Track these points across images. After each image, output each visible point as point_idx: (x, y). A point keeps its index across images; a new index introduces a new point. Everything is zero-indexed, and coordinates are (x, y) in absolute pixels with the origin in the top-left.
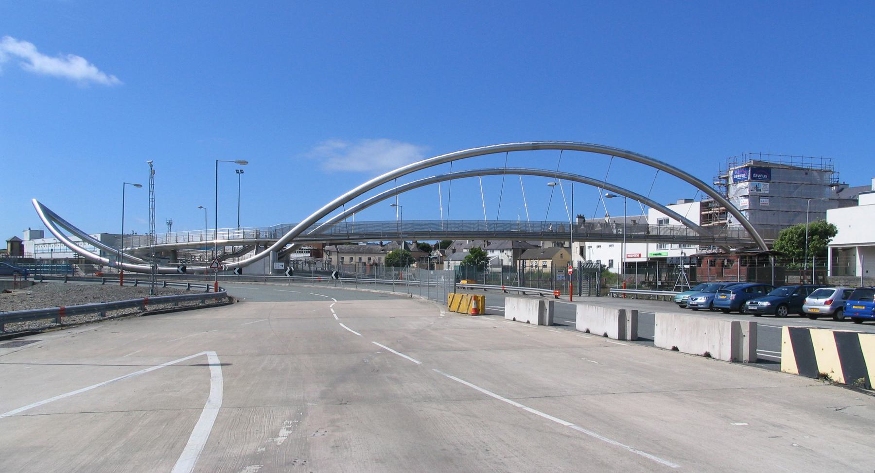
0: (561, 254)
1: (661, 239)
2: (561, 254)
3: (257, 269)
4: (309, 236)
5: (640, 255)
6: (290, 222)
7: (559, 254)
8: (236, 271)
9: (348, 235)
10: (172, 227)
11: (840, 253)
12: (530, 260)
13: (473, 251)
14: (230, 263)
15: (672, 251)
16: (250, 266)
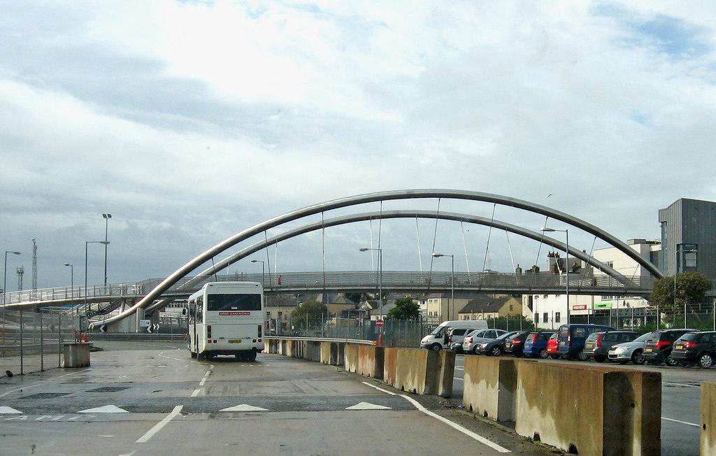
0: (511, 306)
1: (607, 293)
2: (511, 306)
3: (124, 328)
4: (178, 291)
5: (586, 306)
6: (155, 276)
7: (507, 305)
8: (101, 328)
9: (324, 286)
10: (23, 276)
11: (501, 315)
12: (474, 313)
13: (399, 303)
14: (96, 321)
15: (615, 304)
16: (123, 320)
